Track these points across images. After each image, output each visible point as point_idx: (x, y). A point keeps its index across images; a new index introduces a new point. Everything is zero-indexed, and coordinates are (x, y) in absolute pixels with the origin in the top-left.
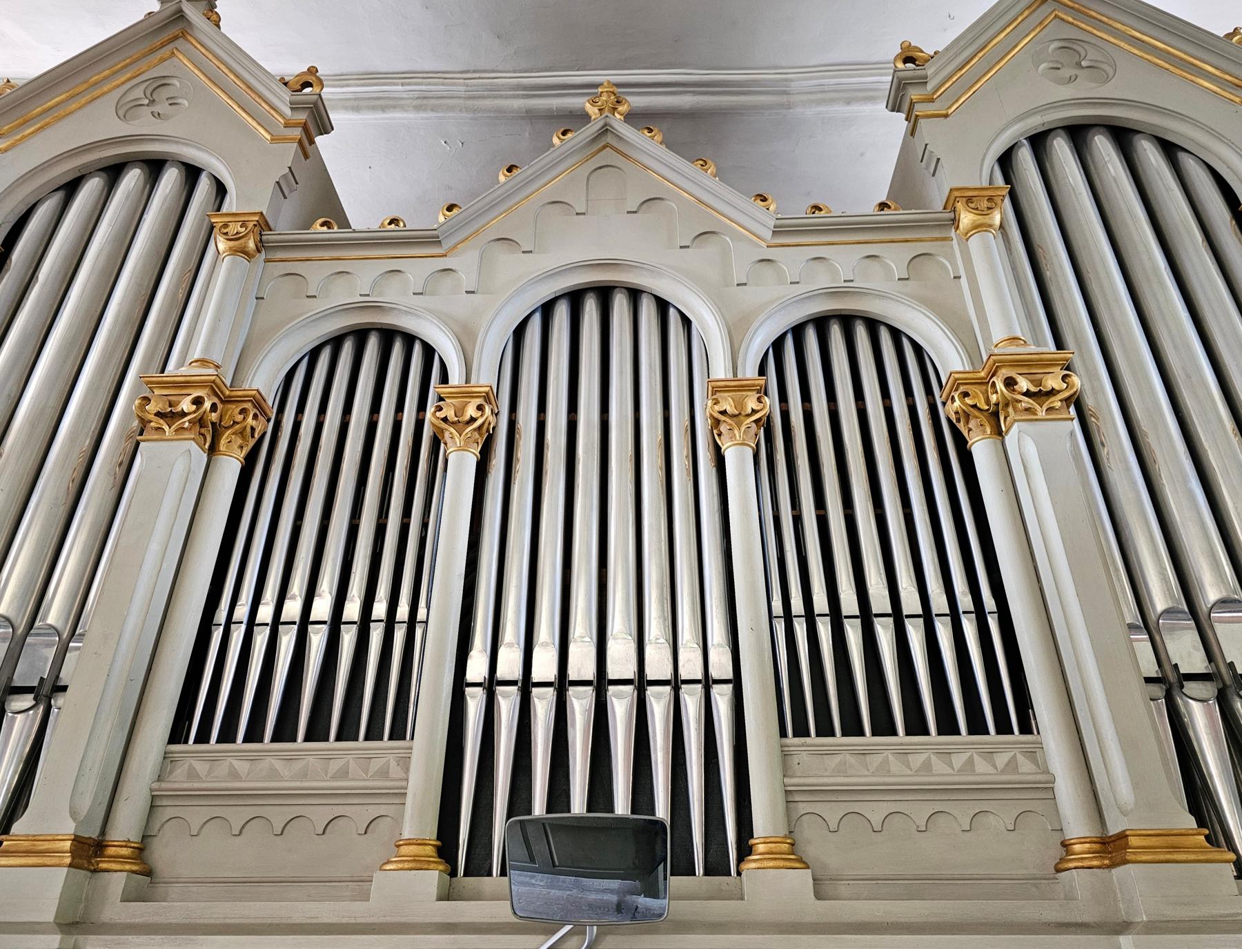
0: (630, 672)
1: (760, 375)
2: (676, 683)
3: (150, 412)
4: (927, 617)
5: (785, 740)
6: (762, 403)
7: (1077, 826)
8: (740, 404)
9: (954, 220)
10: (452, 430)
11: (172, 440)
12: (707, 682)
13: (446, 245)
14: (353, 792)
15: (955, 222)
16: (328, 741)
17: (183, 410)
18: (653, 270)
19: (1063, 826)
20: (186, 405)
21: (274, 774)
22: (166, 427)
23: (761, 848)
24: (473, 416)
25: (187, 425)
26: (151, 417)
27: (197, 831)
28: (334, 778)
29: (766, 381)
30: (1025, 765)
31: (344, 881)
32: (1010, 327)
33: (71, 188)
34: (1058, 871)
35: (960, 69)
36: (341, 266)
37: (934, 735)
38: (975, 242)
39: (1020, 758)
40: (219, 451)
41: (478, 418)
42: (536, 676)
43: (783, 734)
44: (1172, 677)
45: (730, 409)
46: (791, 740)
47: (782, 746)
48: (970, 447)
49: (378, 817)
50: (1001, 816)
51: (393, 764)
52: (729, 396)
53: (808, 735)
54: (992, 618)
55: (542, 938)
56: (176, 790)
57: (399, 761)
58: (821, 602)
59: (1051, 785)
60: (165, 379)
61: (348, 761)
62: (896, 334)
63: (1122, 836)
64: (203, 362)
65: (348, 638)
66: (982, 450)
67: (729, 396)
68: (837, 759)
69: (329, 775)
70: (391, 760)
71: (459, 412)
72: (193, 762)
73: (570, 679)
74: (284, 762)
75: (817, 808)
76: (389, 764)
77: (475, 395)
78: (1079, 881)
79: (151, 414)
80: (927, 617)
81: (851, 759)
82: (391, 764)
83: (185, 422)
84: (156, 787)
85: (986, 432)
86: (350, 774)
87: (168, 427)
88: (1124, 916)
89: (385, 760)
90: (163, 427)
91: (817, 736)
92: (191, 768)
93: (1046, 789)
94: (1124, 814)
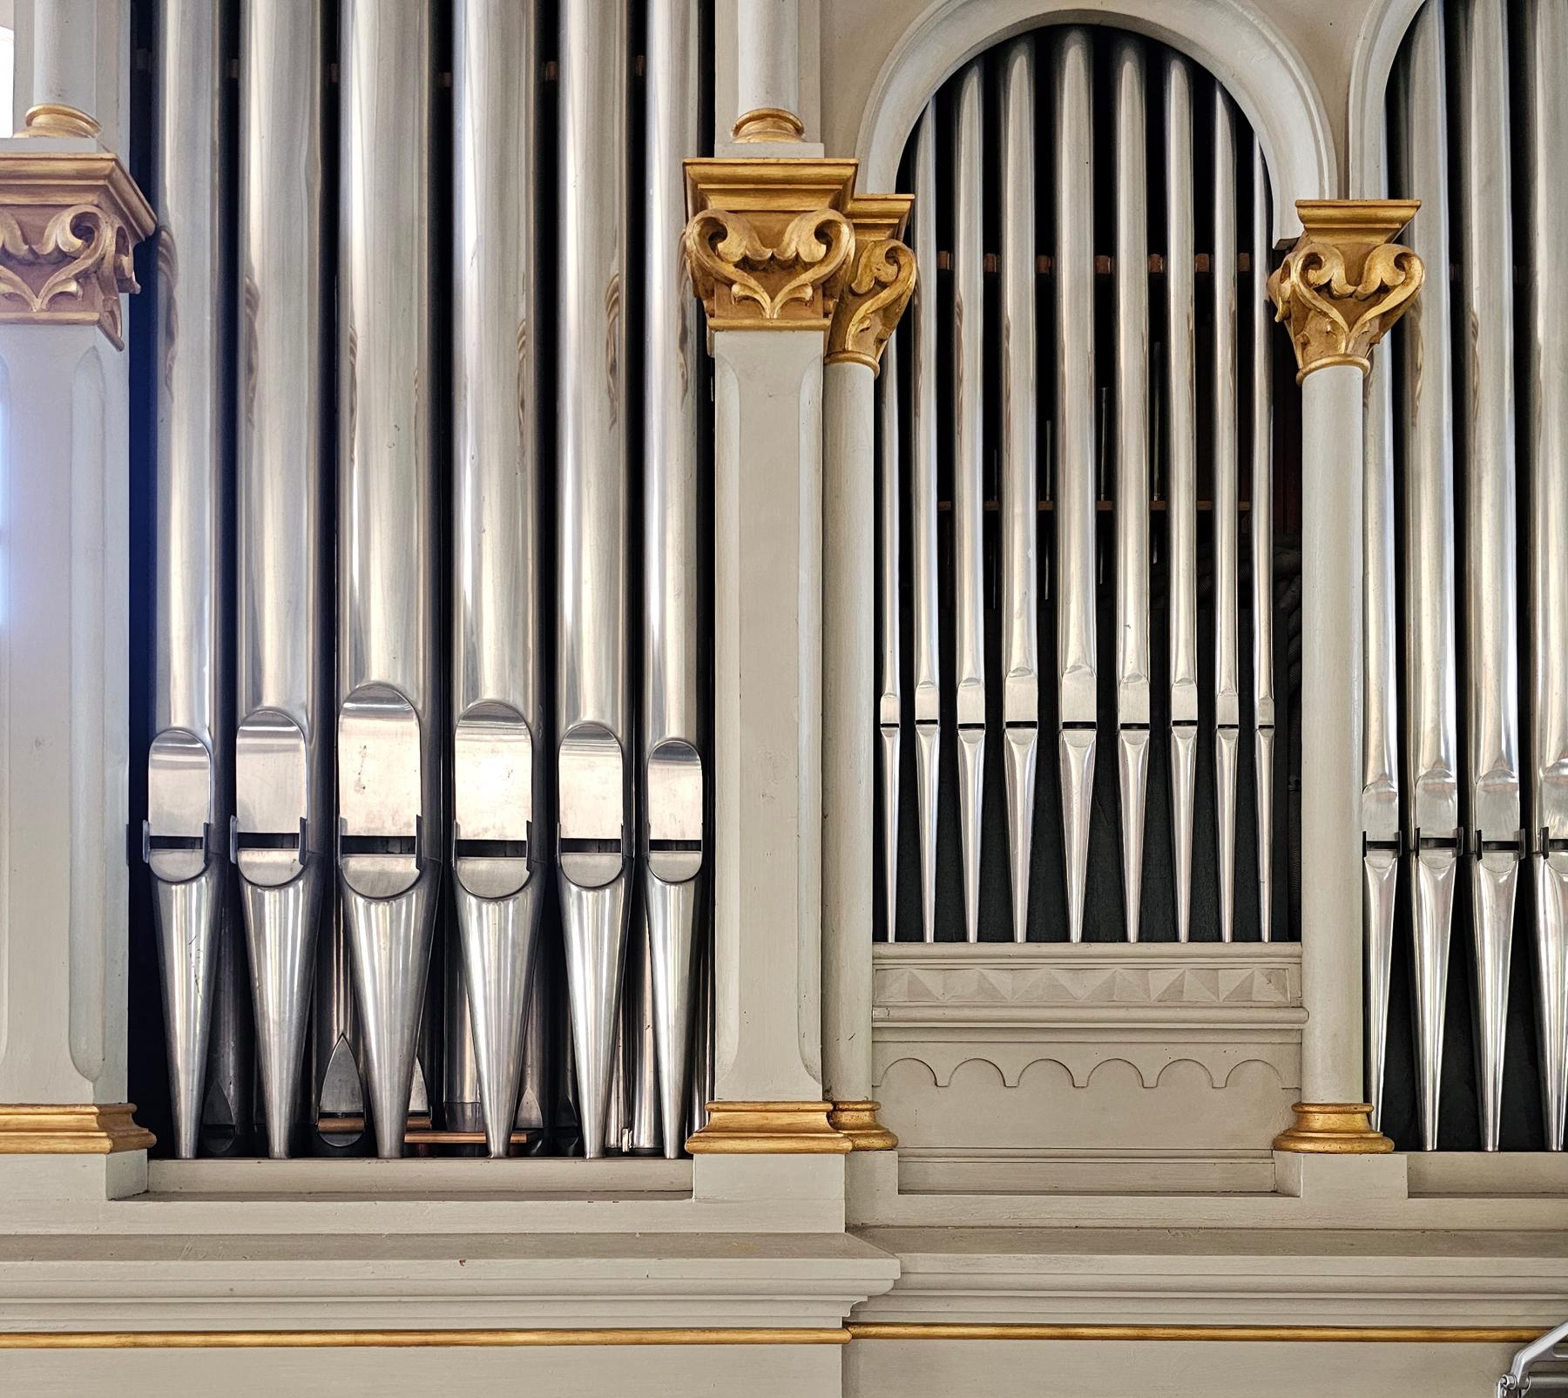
0: (1449, 828)
1: (898, 191)
3: (729, 258)
5: (882, 949)
6: (1404, 269)
8: (1356, 273)
10: (1335, 314)
11: (780, 329)
14: (1212, 1026)
16: (923, 941)
17: (57, 247)
19: (1304, 1085)
20: (60, 234)
22: (763, 297)
24: (1333, 285)
25: (808, 293)
26: (729, 270)
27: (947, 1080)
28: (1162, 1003)
29: (913, 202)
31: (1244, 1157)
32: (773, 83)
37: (1266, 940)
40: (845, 351)
41: (1395, 287)
42: (572, 825)
45: (1339, 282)
46: (892, 947)
47: (874, 958)
48: (1301, 382)
49: (1135, 1067)
51: (1259, 980)
52: (1336, 246)
56: (915, 1021)
57: (1270, 974)
58: (1021, 699)
59: (1301, 1026)
60: (716, 171)
61: (1251, 977)
62: (1203, 84)
64: (773, 119)
67: (1336, 246)
69: (1154, 996)
70: (1257, 974)
71: (1356, 273)
72: (915, 972)
73: (651, 838)
74: (1070, 974)
75: (917, 1051)
76: (1252, 983)
77: (1378, 226)
79: (728, 262)
82: (1256, 982)
83: (805, 285)
84: (882, 1016)
85: (1336, 349)
86: (1184, 995)
87: (768, 299)
89: (1250, 971)
90: (756, 297)
91: (1028, 940)
92: (913, 983)
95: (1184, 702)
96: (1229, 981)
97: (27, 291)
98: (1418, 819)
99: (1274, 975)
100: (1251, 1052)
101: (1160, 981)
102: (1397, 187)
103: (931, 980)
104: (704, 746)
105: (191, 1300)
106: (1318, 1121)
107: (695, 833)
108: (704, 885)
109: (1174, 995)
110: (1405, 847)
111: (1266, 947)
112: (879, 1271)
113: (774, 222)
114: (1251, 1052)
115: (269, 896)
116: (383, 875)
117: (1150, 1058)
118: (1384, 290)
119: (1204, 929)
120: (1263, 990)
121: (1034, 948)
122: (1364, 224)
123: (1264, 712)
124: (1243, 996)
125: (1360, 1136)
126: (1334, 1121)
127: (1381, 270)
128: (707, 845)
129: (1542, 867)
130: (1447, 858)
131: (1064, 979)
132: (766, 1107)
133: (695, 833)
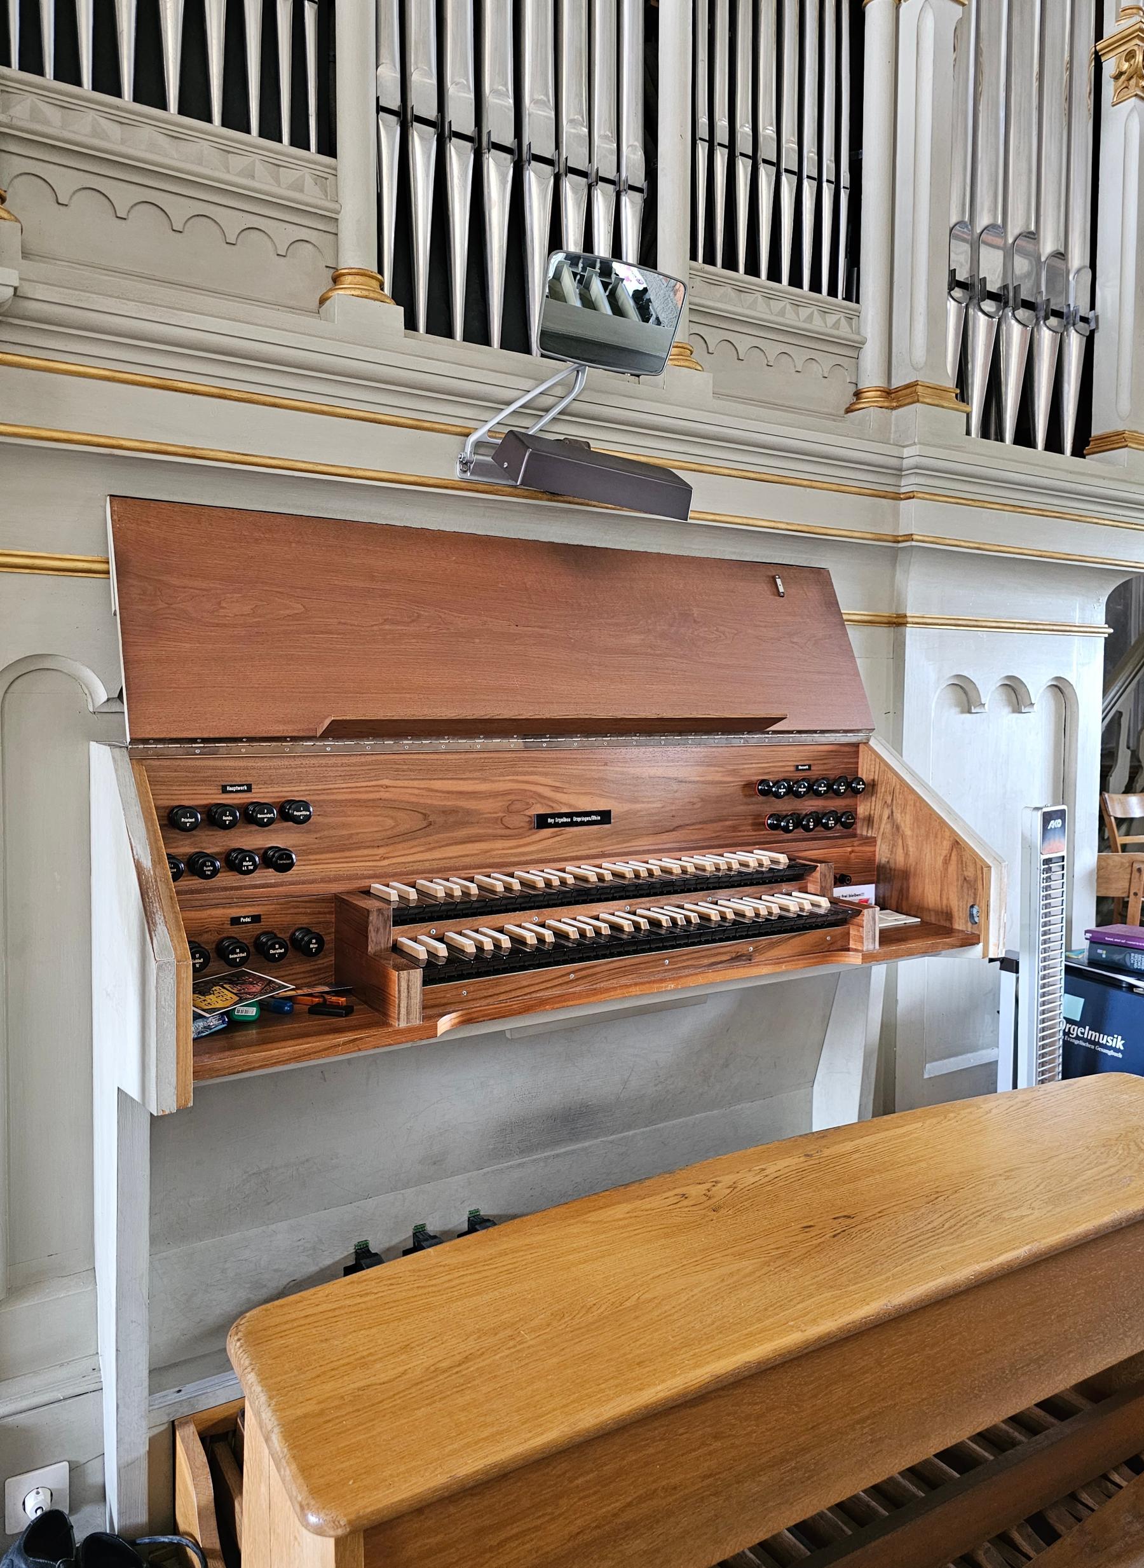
7: (871, 377)
39: (843, 320)
114: (304, 234)
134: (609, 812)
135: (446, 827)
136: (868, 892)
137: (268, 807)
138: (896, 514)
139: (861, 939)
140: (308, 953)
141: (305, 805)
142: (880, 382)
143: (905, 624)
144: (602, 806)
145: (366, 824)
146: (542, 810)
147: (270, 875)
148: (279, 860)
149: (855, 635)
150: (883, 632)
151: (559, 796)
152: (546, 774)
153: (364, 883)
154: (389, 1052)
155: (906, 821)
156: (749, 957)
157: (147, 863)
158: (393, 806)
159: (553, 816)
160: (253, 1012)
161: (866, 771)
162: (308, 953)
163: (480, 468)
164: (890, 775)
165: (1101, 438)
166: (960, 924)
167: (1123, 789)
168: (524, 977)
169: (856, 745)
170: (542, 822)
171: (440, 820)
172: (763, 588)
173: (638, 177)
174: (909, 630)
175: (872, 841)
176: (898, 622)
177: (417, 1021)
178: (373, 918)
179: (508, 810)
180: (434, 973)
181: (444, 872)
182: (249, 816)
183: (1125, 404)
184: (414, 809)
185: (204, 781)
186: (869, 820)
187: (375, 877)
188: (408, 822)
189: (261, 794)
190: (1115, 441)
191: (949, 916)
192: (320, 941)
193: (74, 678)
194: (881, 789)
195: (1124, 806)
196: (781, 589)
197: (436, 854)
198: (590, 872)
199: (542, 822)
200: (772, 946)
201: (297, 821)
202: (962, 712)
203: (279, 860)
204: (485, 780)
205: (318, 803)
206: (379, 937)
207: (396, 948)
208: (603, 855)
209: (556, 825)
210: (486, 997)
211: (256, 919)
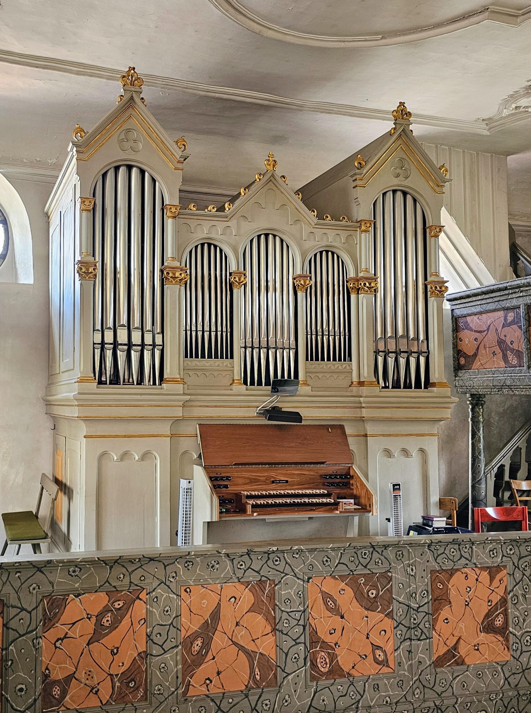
0: (258, 346)
2: (276, 348)
4: (210, 331)
7: (355, 379)
9: (360, 227)
12: (253, 348)
13: (229, 217)
15: (360, 227)
18: (283, 233)
21: (197, 365)
23: (301, 382)
26: (169, 278)
30: (348, 368)
32: (173, 254)
33: (104, 176)
34: (350, 386)
35: (371, 168)
36: (199, 222)
38: (363, 235)
39: (347, 366)
43: (307, 360)
44: (398, 352)
45: (238, 281)
50: (342, 376)
53: (218, 358)
54: (200, 333)
55: (269, 398)
63: (364, 382)
65: (213, 334)
66: (353, 297)
68: (314, 365)
70: (347, 366)
78: (354, 389)
80: (210, 331)
81: (317, 366)
88: (360, 394)
92: (187, 363)
93: (351, 373)
94: (365, 378)
95: (219, 329)
96: (225, 364)
97: (86, 276)
98: (247, 344)
99: (230, 363)
100: (228, 373)
101: (217, 364)
102: (244, 270)
103: (189, 363)
104: (162, 332)
105: (108, 400)
106: (235, 381)
107: (161, 344)
108: (162, 351)
109: (218, 366)
110: (245, 348)
111: (229, 360)
112: (188, 397)
113: (174, 272)
114: (228, 373)
115: (108, 351)
116: (123, 348)
117: (216, 374)
118: (243, 281)
119: (222, 357)
120: (229, 365)
121: (208, 359)
122: (240, 273)
123: (229, 330)
124: (227, 366)
125: (241, 383)
126: (238, 381)
127: (242, 279)
128: (163, 345)
129: (261, 351)
130: (251, 349)
131: (205, 363)
132: (173, 378)
133: (161, 344)
134: (3, 515)
135: (254, 482)
136: (352, 501)
137: (224, 477)
138: (361, 411)
139: (340, 508)
140: (232, 503)
141: (230, 477)
142: (358, 381)
143: (367, 436)
144: (286, 479)
145: (240, 481)
146: (273, 480)
147: (224, 489)
148: (226, 486)
149: (350, 439)
150: (362, 438)
151: (277, 477)
152: (274, 472)
153: (240, 492)
154: (245, 520)
155: (358, 485)
156: (314, 510)
157: (211, 485)
158: (244, 478)
159: (276, 481)
160: (225, 510)
161: (352, 473)
162: (232, 503)
163: (260, 413)
164: (356, 474)
165: (432, 383)
166: (368, 508)
167: (525, 478)
168: (269, 509)
169: (350, 467)
170: (273, 482)
171: (253, 481)
172: (325, 431)
173: (293, 345)
174: (369, 438)
175: (353, 489)
176: (366, 436)
177: (251, 513)
178: (243, 497)
179: (266, 479)
180: (253, 506)
181: (254, 491)
182: (222, 479)
183: (437, 375)
184: (248, 478)
185: (214, 473)
186: (352, 484)
187: (242, 491)
188: (248, 481)
189: (223, 475)
190: (434, 385)
191: (366, 506)
192: (234, 501)
193: (191, 454)
194: (354, 477)
195: (520, 485)
196: (330, 431)
197: (252, 487)
198: (282, 492)
199: (273, 482)
200: (319, 508)
201: (229, 480)
202: (388, 458)
203: (226, 486)
204: (261, 473)
205: (232, 477)
206: (244, 500)
207: (246, 502)
208: (286, 489)
209: (276, 483)
210: (310, 108)
211: (223, 496)
